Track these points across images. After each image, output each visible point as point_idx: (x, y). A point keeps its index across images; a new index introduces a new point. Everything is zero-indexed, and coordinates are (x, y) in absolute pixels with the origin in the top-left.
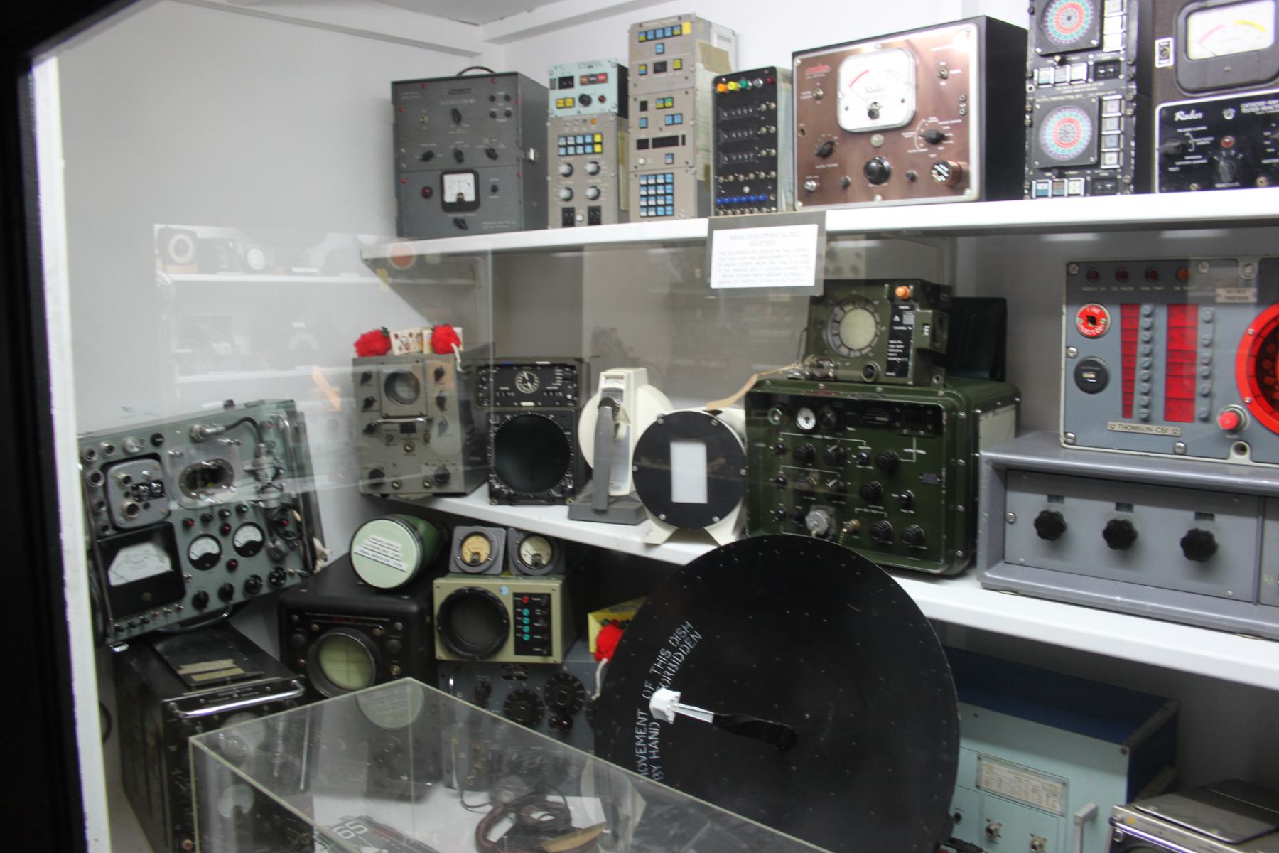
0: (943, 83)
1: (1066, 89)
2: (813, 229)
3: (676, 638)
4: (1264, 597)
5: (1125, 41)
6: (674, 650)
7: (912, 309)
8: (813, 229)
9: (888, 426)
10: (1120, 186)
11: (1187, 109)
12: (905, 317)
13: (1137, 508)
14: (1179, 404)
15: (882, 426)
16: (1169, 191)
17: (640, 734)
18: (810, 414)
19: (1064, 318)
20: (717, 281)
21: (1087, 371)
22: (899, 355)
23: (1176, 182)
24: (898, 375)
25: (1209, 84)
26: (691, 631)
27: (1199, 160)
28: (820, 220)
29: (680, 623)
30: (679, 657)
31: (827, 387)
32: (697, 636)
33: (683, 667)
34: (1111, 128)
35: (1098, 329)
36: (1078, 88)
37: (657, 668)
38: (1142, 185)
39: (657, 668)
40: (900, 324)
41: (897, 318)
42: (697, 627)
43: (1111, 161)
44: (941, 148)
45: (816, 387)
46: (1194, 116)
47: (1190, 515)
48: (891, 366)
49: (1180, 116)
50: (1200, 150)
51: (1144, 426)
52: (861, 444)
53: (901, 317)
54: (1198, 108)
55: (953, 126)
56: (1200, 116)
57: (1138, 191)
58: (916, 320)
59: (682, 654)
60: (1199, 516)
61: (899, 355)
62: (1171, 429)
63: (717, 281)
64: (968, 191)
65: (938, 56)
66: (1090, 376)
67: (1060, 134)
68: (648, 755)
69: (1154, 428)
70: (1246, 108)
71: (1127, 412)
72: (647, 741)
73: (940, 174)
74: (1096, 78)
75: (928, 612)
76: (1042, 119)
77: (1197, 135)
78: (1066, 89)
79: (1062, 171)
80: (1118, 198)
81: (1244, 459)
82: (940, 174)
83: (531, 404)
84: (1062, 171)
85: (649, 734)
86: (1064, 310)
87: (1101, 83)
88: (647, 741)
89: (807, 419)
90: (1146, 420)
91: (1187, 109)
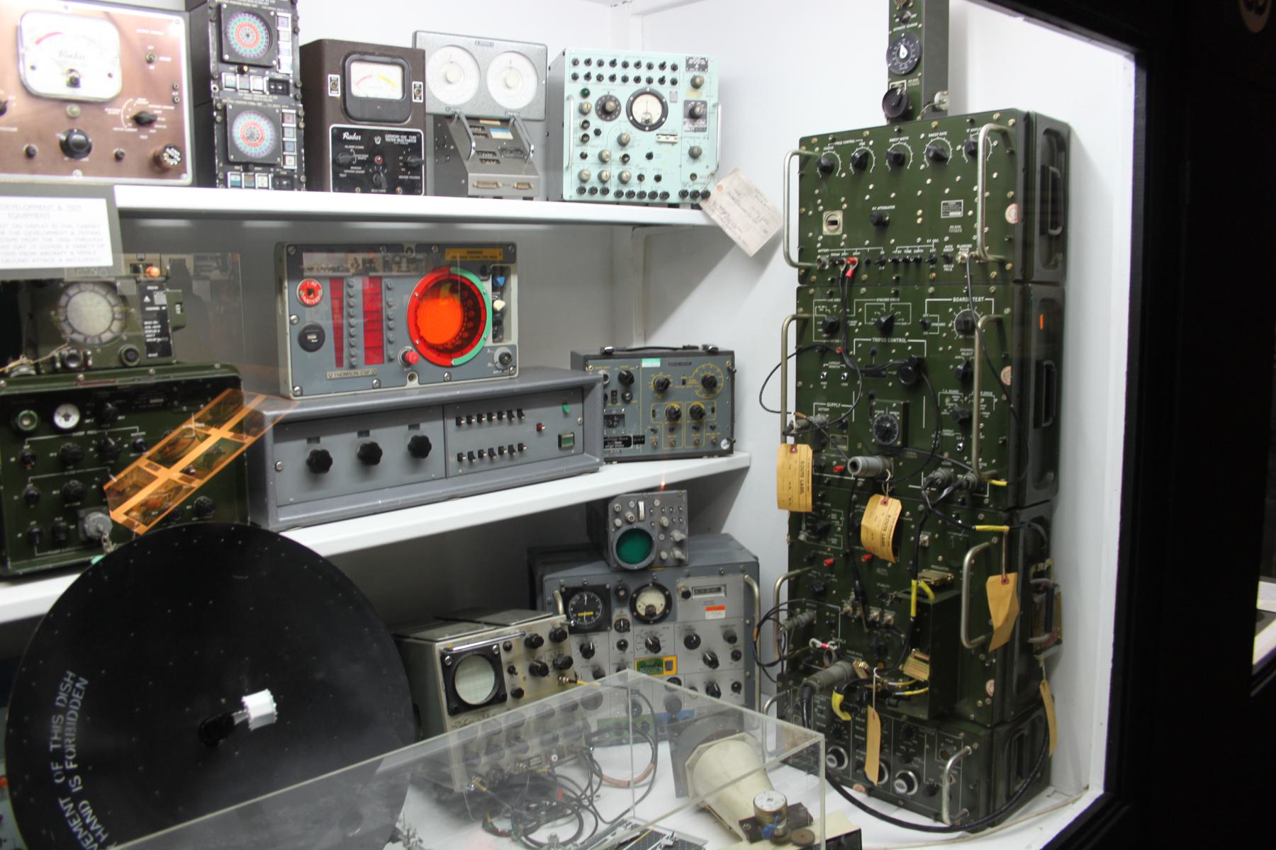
0: (152, 67)
1: (248, 96)
2: (101, 204)
3: (62, 696)
4: (451, 473)
5: (293, 67)
6: (64, 711)
7: (161, 288)
8: (101, 204)
9: (164, 407)
10: (296, 184)
11: (351, 131)
12: (156, 297)
13: (372, 432)
14: (375, 350)
15: (158, 408)
16: (340, 191)
17: (76, 825)
18: (63, 410)
19: (286, 291)
20: (305, 255)
21: (311, 333)
22: (157, 336)
23: (345, 185)
24: (161, 355)
25: (367, 116)
26: (76, 680)
27: (359, 170)
28: (107, 193)
29: (60, 678)
30: (72, 716)
31: (87, 377)
32: (82, 683)
33: (80, 723)
34: (291, 137)
35: (317, 300)
36: (258, 96)
37: (55, 742)
38: (314, 181)
39: (55, 742)
40: (152, 304)
41: (147, 299)
42: (79, 674)
43: (291, 163)
44: (152, 131)
45: (75, 379)
46: (355, 137)
47: (355, 435)
48: (151, 347)
49: (346, 135)
50: (360, 163)
51: (352, 372)
52: (135, 431)
53: (151, 297)
54: (359, 132)
55: (164, 111)
56: (359, 138)
57: (310, 187)
58: (168, 298)
59: (74, 710)
60: (411, 427)
61: (157, 336)
62: (370, 369)
63: (305, 255)
64: (184, 176)
65: (144, 38)
66: (313, 338)
67: (249, 134)
68: (97, 840)
69: (360, 372)
70: (389, 138)
71: (339, 363)
72: (86, 827)
73: (171, 157)
74: (273, 92)
75: (323, 552)
76: (234, 119)
77: (358, 152)
78: (248, 96)
79: (248, 166)
80: (295, 193)
81: (415, 383)
82: (171, 157)
83: (152, 401)
84: (248, 166)
85: (83, 819)
86: (286, 284)
87: (276, 97)
88: (86, 827)
89: (67, 417)
90: (352, 367)
91: (351, 131)
